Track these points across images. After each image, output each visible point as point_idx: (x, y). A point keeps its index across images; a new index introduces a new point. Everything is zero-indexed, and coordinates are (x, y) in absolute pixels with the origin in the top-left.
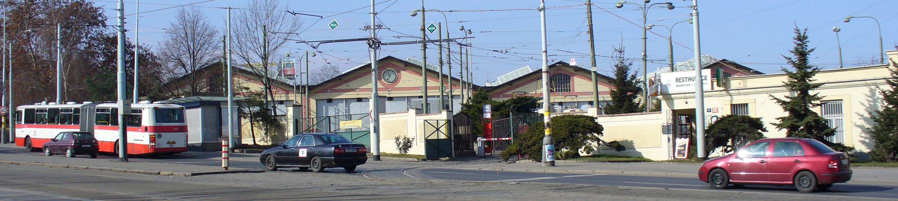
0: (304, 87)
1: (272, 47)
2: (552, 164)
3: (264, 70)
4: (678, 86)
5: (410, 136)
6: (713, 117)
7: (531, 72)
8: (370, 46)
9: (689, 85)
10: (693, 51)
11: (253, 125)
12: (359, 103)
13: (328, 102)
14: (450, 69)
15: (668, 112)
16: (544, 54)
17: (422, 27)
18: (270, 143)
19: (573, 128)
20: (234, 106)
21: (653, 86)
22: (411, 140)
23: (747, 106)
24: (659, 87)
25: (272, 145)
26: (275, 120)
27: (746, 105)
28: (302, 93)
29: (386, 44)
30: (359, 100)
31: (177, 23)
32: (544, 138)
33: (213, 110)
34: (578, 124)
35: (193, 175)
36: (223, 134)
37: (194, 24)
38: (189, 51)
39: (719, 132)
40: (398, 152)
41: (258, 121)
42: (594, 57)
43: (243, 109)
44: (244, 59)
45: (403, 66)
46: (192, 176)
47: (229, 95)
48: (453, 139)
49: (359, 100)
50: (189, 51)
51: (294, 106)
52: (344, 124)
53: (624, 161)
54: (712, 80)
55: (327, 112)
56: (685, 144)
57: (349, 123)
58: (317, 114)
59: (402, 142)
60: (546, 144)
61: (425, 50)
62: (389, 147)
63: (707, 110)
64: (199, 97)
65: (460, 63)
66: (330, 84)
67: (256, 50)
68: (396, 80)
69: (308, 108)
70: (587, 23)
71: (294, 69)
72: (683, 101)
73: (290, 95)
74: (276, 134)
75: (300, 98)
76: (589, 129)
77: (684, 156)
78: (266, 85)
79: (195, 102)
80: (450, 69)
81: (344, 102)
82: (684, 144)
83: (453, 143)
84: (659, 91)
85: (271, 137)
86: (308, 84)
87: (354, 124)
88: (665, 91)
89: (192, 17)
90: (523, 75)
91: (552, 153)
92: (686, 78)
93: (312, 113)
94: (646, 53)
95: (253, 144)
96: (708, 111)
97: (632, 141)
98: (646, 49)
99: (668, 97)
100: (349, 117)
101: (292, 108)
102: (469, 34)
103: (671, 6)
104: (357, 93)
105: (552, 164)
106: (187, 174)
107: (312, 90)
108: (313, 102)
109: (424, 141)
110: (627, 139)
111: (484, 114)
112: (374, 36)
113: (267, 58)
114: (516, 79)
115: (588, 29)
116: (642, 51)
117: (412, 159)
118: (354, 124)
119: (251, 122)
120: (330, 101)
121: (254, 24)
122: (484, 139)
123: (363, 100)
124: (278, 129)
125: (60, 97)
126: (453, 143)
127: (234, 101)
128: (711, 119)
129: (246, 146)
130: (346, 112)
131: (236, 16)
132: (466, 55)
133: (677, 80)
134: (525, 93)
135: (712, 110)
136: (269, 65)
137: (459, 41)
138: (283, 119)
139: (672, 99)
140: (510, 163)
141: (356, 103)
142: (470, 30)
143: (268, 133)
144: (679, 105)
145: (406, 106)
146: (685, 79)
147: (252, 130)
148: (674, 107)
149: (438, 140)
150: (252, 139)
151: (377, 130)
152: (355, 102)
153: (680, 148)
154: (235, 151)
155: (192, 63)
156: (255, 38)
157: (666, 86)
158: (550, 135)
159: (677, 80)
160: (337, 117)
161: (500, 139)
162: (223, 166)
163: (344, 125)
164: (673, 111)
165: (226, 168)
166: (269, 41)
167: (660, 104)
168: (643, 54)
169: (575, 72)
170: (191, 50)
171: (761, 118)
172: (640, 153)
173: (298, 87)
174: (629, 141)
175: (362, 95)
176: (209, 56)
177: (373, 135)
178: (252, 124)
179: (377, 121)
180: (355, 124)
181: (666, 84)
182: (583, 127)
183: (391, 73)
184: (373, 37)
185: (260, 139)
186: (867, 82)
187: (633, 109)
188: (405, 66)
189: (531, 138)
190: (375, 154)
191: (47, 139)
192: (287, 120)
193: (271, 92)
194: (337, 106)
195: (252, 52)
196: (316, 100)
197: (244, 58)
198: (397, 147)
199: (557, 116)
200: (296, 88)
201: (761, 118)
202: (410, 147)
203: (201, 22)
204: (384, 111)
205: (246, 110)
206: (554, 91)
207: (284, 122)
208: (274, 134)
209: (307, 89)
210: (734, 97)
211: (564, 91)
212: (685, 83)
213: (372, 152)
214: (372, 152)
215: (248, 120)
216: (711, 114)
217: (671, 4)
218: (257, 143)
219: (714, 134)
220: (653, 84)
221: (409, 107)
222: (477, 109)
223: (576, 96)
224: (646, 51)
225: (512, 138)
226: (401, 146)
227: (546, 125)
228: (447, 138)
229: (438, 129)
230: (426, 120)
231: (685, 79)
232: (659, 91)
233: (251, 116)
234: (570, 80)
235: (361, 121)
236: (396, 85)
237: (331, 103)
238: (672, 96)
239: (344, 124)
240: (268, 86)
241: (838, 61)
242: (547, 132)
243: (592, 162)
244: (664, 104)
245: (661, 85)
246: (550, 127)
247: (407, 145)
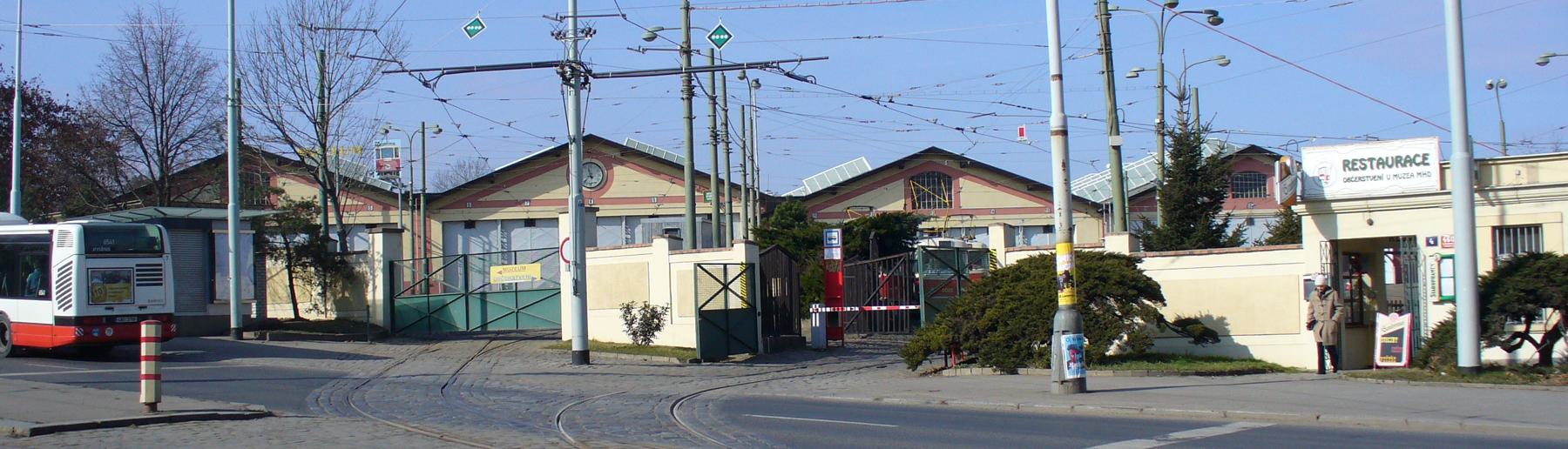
0: (417, 196)
1: (336, 98)
2: (1080, 385)
3: (318, 149)
4: (1349, 180)
5: (657, 301)
6: (1443, 258)
7: (870, 169)
8: (566, 81)
9: (1380, 178)
10: (1050, 152)
11: (294, 275)
12: (528, 230)
13: (466, 228)
14: (728, 153)
15: (1323, 244)
16: (1054, 85)
17: (685, 46)
18: (332, 316)
19: (1096, 286)
20: (242, 232)
21: (1288, 181)
22: (659, 310)
23: (1537, 232)
24: (1299, 183)
25: (336, 319)
26: (343, 262)
27: (1537, 228)
28: (413, 209)
29: (604, 76)
30: (530, 223)
31: (125, 46)
32: (1057, 315)
33: (194, 240)
34: (1105, 275)
35: (35, 432)
36: (217, 297)
37: (164, 48)
38: (152, 108)
39: (1519, 300)
40: (627, 339)
41: (304, 265)
42: (1116, 113)
43: (271, 239)
44: (273, 125)
45: (616, 154)
46: (32, 435)
47: (231, 205)
48: (759, 309)
49: (530, 223)
50: (152, 108)
51: (384, 231)
52: (500, 273)
53: (1232, 373)
54: (1441, 165)
55: (466, 244)
56: (1402, 329)
57: (511, 271)
58: (444, 250)
59: (639, 317)
60: (1064, 332)
61: (690, 100)
62: (609, 328)
64: (160, 209)
65: (741, 144)
66: (476, 190)
67: (302, 104)
68: (604, 184)
69: (425, 237)
70: (1097, 27)
71: (398, 161)
72: (1360, 219)
73: (391, 213)
74: (347, 295)
75: (409, 218)
76: (1134, 287)
77: (1399, 360)
78: (323, 185)
79: (152, 219)
80: (728, 153)
81: (499, 226)
82: (1400, 327)
83: (759, 319)
84: (1299, 193)
85: (336, 302)
86: (424, 190)
87: (522, 273)
88: (1312, 192)
89: (158, 30)
90: (855, 175)
91: (1079, 356)
92: (1371, 160)
93: (433, 249)
94: (1163, 118)
95: (293, 317)
96: (1428, 244)
97: (1223, 319)
98: (1163, 111)
99: (1321, 208)
100: (509, 256)
101: (381, 234)
102: (756, 88)
103: (1215, 19)
104: (526, 209)
105: (1080, 385)
106: (19, 431)
107: (433, 202)
108: (436, 228)
109: (694, 314)
110: (1211, 313)
111: (826, 250)
112: (575, 56)
113: (328, 123)
114: (860, 176)
115: (1099, 43)
116: (1155, 115)
117: (666, 359)
118: (522, 273)
119: (288, 267)
120: (470, 224)
121: (298, 45)
122: (828, 310)
123: (477, 225)
124: (351, 283)
126: (759, 319)
127: (244, 220)
128: (1439, 262)
129: (276, 324)
130: (503, 248)
131: (257, 29)
133: (1346, 164)
134: (871, 208)
136: (330, 139)
137: (787, 67)
138: (361, 260)
139: (1333, 214)
140: (926, 374)
141: (523, 229)
142: (757, 81)
143: (328, 294)
144: (1351, 228)
145: (624, 236)
146: (1368, 163)
147: (291, 286)
148: (1336, 234)
149: (727, 312)
150: (291, 305)
151: (580, 288)
152: (521, 227)
153: (1387, 340)
154: (245, 335)
155: (159, 135)
156: (299, 77)
157: (1316, 181)
158: (1072, 307)
159: (1346, 164)
160: (487, 257)
161: (867, 308)
162: (143, 399)
163: (500, 275)
164: (1332, 242)
165: (152, 406)
166: (330, 82)
167: (1299, 227)
168: (1158, 121)
169: (962, 169)
170: (156, 106)
172: (1245, 348)
173: (405, 196)
174: (1215, 318)
175: (535, 213)
176: (198, 118)
177: (568, 300)
178: (290, 273)
179: (580, 265)
180: (526, 274)
181: (1316, 174)
182: (1120, 283)
183: (594, 169)
184: (571, 57)
185: (308, 305)
186: (1371, 202)
187: (1214, 240)
188: (622, 155)
189: (983, 311)
190: (576, 347)
191: (174, 278)
192: (371, 263)
193: (335, 201)
194: (488, 238)
195: (291, 108)
196: (443, 223)
197: (273, 122)
198: (626, 327)
199: (1041, 255)
200: (402, 200)
202: (658, 328)
203: (181, 42)
204: (593, 244)
205: (279, 240)
206: (945, 204)
207: (363, 268)
208: (341, 295)
209: (422, 198)
210: (1507, 206)
211: (940, 206)
212: (1368, 172)
213: (565, 338)
214: (566, 336)
215: (281, 264)
216: (1438, 250)
217: (1215, 13)
218: (302, 315)
219: (1504, 305)
220: (1289, 173)
221: (629, 236)
222: (791, 240)
223: (971, 216)
224: (1163, 114)
225: (922, 307)
226: (635, 326)
227: (1061, 279)
228: (745, 306)
229: (726, 287)
230: (699, 265)
231: (1368, 163)
232: (1299, 193)
233: (289, 255)
234: (950, 184)
235: (538, 265)
236: (602, 194)
237: (472, 230)
238: (1334, 205)
239: (500, 273)
240: (329, 188)
241: (1564, 141)
242: (1064, 298)
243: (1154, 375)
244: (1309, 226)
245: (1304, 178)
246: (1073, 286)
247: (651, 322)
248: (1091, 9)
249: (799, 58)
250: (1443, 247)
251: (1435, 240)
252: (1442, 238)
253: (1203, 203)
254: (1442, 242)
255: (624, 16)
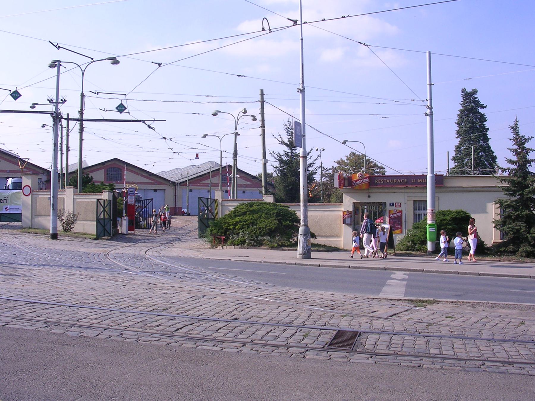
13: (154, 192)
63: (390, 204)
125: (329, 208)
132: (79, 67)
135: (395, 205)
171: (456, 123)
201: (456, 123)
248: (1, 172)
249: (154, 120)
250: (396, 207)
251: (393, 204)
252: (396, 203)
253: (517, 175)
254: (396, 205)
255: (129, 113)
